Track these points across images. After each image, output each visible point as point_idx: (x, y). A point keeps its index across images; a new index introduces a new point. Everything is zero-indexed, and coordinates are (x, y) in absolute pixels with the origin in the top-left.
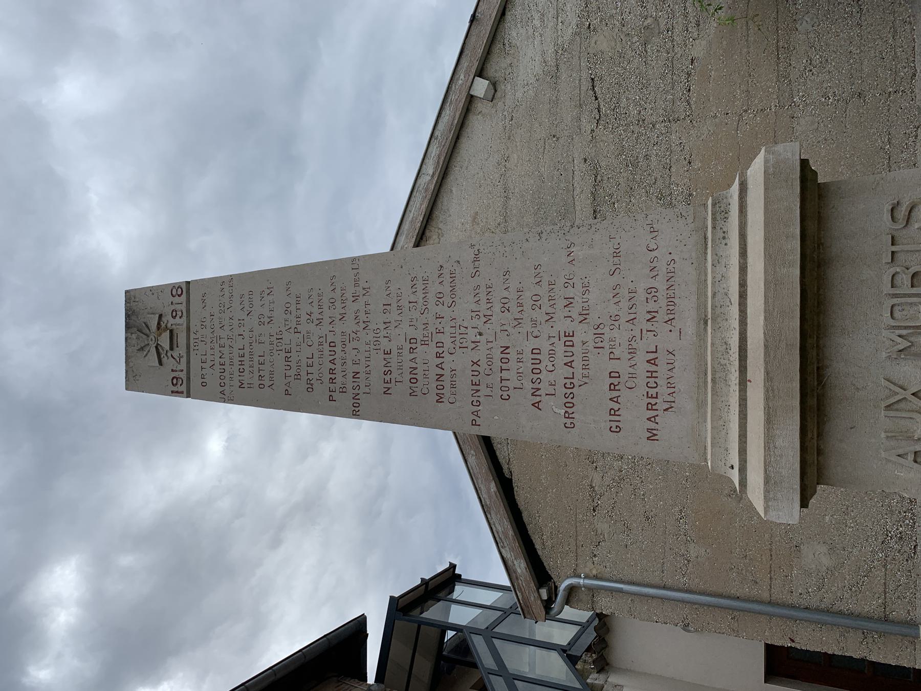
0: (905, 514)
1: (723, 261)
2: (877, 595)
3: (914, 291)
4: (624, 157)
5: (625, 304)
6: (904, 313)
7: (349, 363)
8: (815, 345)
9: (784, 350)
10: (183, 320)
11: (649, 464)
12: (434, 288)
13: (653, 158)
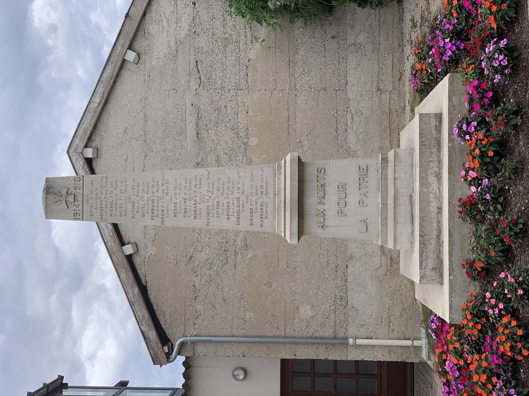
1: (280, 179)
2: (332, 327)
3: (321, 189)
4: (213, 106)
5: (254, 190)
7: (160, 207)
10: (81, 191)
12: (193, 182)
13: (229, 108)
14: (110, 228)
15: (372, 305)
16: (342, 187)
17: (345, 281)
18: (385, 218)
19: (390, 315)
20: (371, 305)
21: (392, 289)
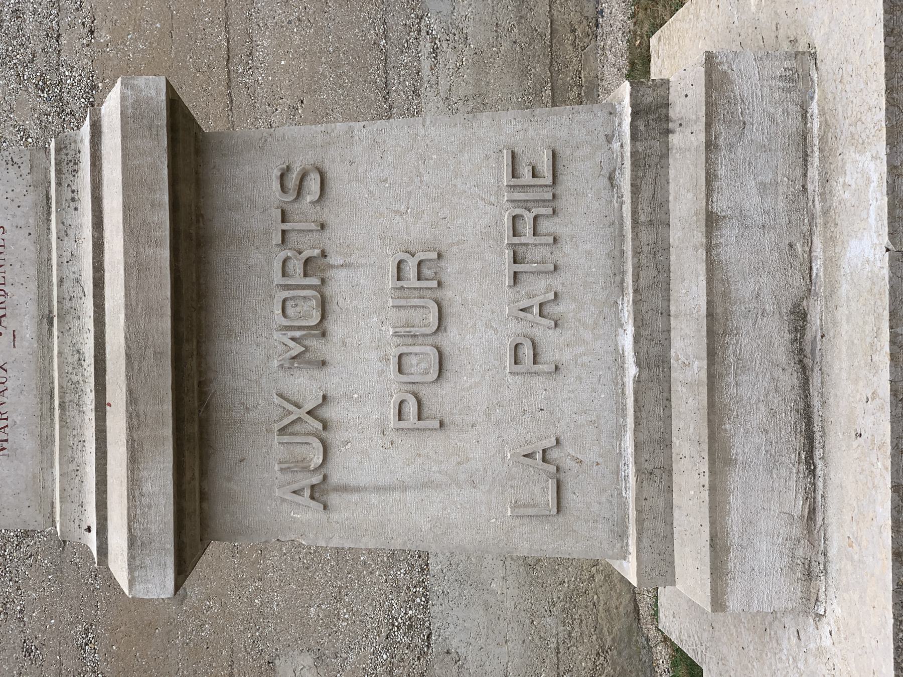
0: (414, 590)
1: (72, 233)
6: (298, 309)
8: (195, 353)
9: (152, 361)
11: (31, 556)
15: (506, 642)
17: (423, 570)
18: (657, 436)
19: (562, 669)
20: (502, 641)
21: (565, 589)
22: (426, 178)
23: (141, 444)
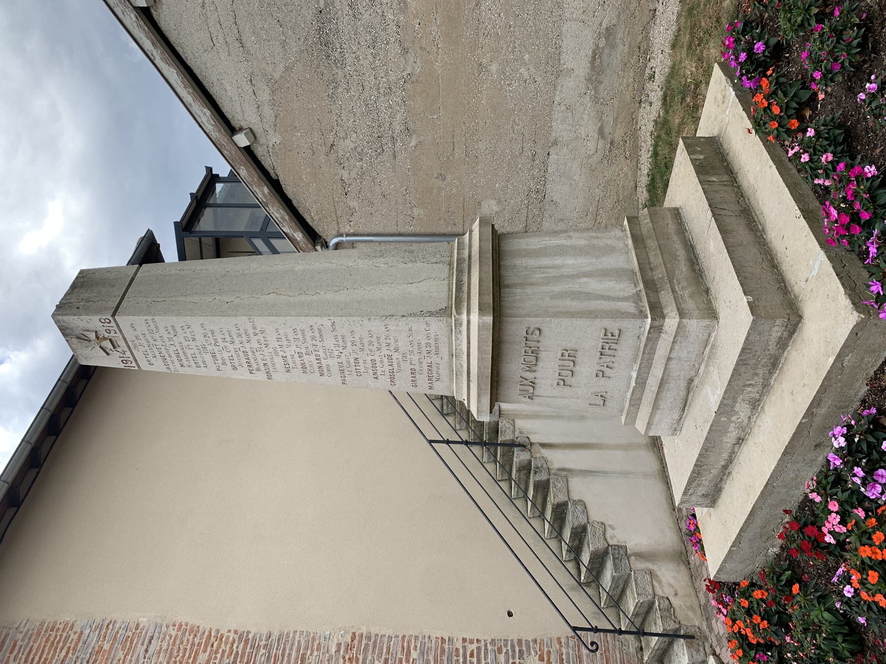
7: (259, 360)
12: (309, 334)
14: (208, 114)
16: (570, 356)
19: (599, 207)
22: (575, 333)
23: (481, 394)
